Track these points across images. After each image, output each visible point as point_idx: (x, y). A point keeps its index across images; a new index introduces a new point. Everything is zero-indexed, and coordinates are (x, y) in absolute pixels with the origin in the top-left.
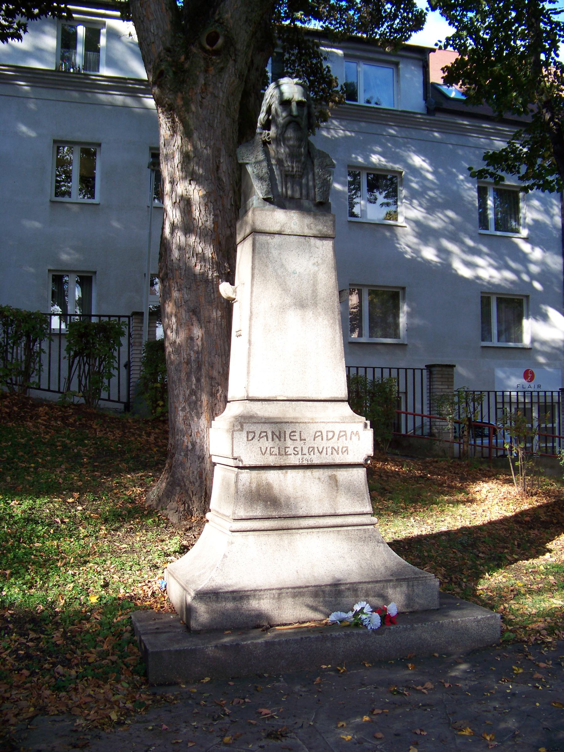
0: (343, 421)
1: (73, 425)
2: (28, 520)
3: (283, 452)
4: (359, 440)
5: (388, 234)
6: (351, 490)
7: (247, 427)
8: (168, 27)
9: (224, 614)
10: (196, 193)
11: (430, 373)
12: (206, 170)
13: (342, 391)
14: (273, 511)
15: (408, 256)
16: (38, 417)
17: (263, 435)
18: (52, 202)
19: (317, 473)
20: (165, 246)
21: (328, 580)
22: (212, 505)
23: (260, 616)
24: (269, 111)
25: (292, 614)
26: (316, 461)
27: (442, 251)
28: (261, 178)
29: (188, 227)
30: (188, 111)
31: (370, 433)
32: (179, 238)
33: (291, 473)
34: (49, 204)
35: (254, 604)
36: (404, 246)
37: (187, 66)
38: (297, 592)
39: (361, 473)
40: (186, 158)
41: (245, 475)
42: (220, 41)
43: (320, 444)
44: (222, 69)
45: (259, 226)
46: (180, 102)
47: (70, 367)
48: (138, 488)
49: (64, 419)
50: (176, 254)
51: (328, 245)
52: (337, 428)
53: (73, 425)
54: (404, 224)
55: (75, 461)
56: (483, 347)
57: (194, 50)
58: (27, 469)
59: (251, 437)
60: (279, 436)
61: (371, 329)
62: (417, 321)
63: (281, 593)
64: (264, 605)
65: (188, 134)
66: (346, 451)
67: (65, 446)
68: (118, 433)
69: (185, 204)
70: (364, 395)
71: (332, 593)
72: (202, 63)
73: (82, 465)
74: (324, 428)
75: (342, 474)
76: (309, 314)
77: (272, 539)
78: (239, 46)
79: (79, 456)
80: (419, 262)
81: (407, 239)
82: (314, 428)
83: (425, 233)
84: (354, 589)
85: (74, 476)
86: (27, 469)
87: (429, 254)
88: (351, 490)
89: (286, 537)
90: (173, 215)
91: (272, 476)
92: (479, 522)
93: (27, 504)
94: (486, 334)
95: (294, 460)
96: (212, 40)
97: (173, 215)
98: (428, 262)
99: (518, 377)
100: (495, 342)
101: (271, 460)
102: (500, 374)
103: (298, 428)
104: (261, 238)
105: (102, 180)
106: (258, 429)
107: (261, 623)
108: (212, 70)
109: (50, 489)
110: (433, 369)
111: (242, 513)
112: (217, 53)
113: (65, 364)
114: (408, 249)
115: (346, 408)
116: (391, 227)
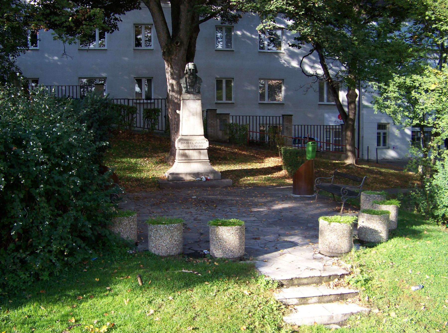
0: (202, 140)
1: (146, 140)
2: (135, 164)
3: (189, 146)
4: (205, 144)
5: (277, 57)
6: (204, 154)
7: (181, 141)
8: (166, 38)
9: (175, 177)
10: (174, 82)
11: (283, 118)
12: (177, 76)
13: (203, 133)
14: (187, 158)
15: (285, 66)
16: (135, 138)
17: (184, 143)
18: (134, 50)
19: (196, 151)
20: (168, 95)
21: (197, 172)
22: (176, 158)
23: (182, 178)
24: (187, 71)
25: (188, 178)
26: (196, 148)
27: (301, 63)
28: (184, 88)
29: (173, 90)
30: (171, 61)
31: (208, 142)
32: (171, 93)
33: (190, 151)
34: (133, 50)
35: (181, 176)
36: (283, 61)
37: (171, 49)
38: (190, 174)
39: (206, 151)
40: (172, 74)
41: (181, 151)
42: (179, 44)
43: (196, 145)
44: (180, 50)
45: (184, 98)
46: (169, 59)
47: (144, 123)
48: (162, 156)
49: (143, 138)
50: (170, 97)
51: (200, 101)
52: (201, 141)
53: (146, 140)
54: (284, 52)
55: (146, 150)
56: (319, 105)
57: (173, 45)
58: (134, 152)
59: (182, 143)
60: (188, 143)
61: (269, 98)
62: (290, 93)
63: (186, 174)
64: (183, 176)
65: (172, 68)
66: (203, 146)
67: (143, 146)
68: (159, 142)
69: (172, 85)
70: (206, 135)
71: (197, 175)
72: (175, 49)
73: (148, 151)
74: (198, 141)
75: (202, 151)
76: (195, 117)
77: (186, 164)
78: (185, 43)
79: (147, 149)
80: (290, 68)
81: (285, 58)
82: (195, 141)
83: (292, 55)
84: (202, 174)
85: (146, 154)
86: (134, 152)
87: (295, 64)
88: (204, 154)
89: (189, 164)
90: (169, 88)
91: (187, 151)
92: (266, 167)
93: (135, 160)
94: (321, 99)
95: (191, 148)
96: (177, 43)
97: (169, 88)
98: (294, 68)
99: (335, 117)
100: (325, 102)
101: (186, 148)
102: (326, 116)
103: (192, 141)
104: (185, 101)
105: (154, 40)
106: (183, 141)
107: (181, 179)
108: (177, 51)
109: (141, 157)
110: (284, 117)
111: (180, 159)
112: (178, 46)
113: (142, 121)
114: (286, 63)
115: (203, 137)
116: (277, 53)
